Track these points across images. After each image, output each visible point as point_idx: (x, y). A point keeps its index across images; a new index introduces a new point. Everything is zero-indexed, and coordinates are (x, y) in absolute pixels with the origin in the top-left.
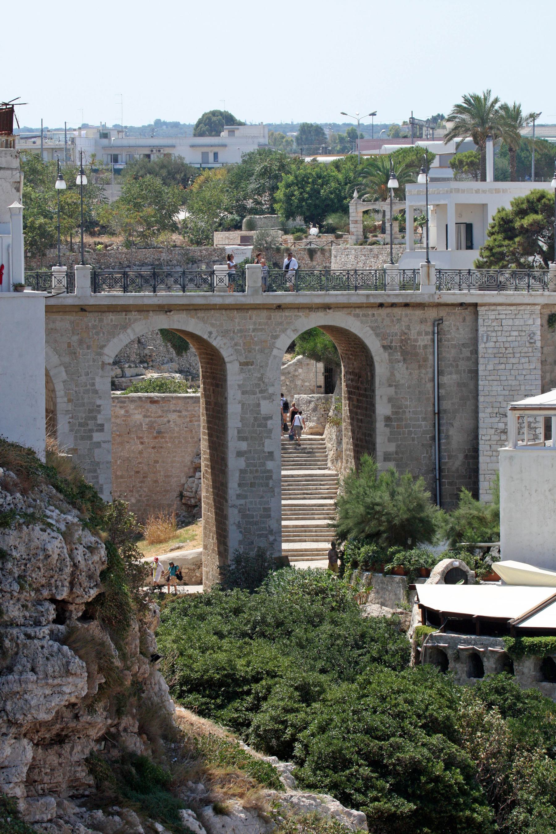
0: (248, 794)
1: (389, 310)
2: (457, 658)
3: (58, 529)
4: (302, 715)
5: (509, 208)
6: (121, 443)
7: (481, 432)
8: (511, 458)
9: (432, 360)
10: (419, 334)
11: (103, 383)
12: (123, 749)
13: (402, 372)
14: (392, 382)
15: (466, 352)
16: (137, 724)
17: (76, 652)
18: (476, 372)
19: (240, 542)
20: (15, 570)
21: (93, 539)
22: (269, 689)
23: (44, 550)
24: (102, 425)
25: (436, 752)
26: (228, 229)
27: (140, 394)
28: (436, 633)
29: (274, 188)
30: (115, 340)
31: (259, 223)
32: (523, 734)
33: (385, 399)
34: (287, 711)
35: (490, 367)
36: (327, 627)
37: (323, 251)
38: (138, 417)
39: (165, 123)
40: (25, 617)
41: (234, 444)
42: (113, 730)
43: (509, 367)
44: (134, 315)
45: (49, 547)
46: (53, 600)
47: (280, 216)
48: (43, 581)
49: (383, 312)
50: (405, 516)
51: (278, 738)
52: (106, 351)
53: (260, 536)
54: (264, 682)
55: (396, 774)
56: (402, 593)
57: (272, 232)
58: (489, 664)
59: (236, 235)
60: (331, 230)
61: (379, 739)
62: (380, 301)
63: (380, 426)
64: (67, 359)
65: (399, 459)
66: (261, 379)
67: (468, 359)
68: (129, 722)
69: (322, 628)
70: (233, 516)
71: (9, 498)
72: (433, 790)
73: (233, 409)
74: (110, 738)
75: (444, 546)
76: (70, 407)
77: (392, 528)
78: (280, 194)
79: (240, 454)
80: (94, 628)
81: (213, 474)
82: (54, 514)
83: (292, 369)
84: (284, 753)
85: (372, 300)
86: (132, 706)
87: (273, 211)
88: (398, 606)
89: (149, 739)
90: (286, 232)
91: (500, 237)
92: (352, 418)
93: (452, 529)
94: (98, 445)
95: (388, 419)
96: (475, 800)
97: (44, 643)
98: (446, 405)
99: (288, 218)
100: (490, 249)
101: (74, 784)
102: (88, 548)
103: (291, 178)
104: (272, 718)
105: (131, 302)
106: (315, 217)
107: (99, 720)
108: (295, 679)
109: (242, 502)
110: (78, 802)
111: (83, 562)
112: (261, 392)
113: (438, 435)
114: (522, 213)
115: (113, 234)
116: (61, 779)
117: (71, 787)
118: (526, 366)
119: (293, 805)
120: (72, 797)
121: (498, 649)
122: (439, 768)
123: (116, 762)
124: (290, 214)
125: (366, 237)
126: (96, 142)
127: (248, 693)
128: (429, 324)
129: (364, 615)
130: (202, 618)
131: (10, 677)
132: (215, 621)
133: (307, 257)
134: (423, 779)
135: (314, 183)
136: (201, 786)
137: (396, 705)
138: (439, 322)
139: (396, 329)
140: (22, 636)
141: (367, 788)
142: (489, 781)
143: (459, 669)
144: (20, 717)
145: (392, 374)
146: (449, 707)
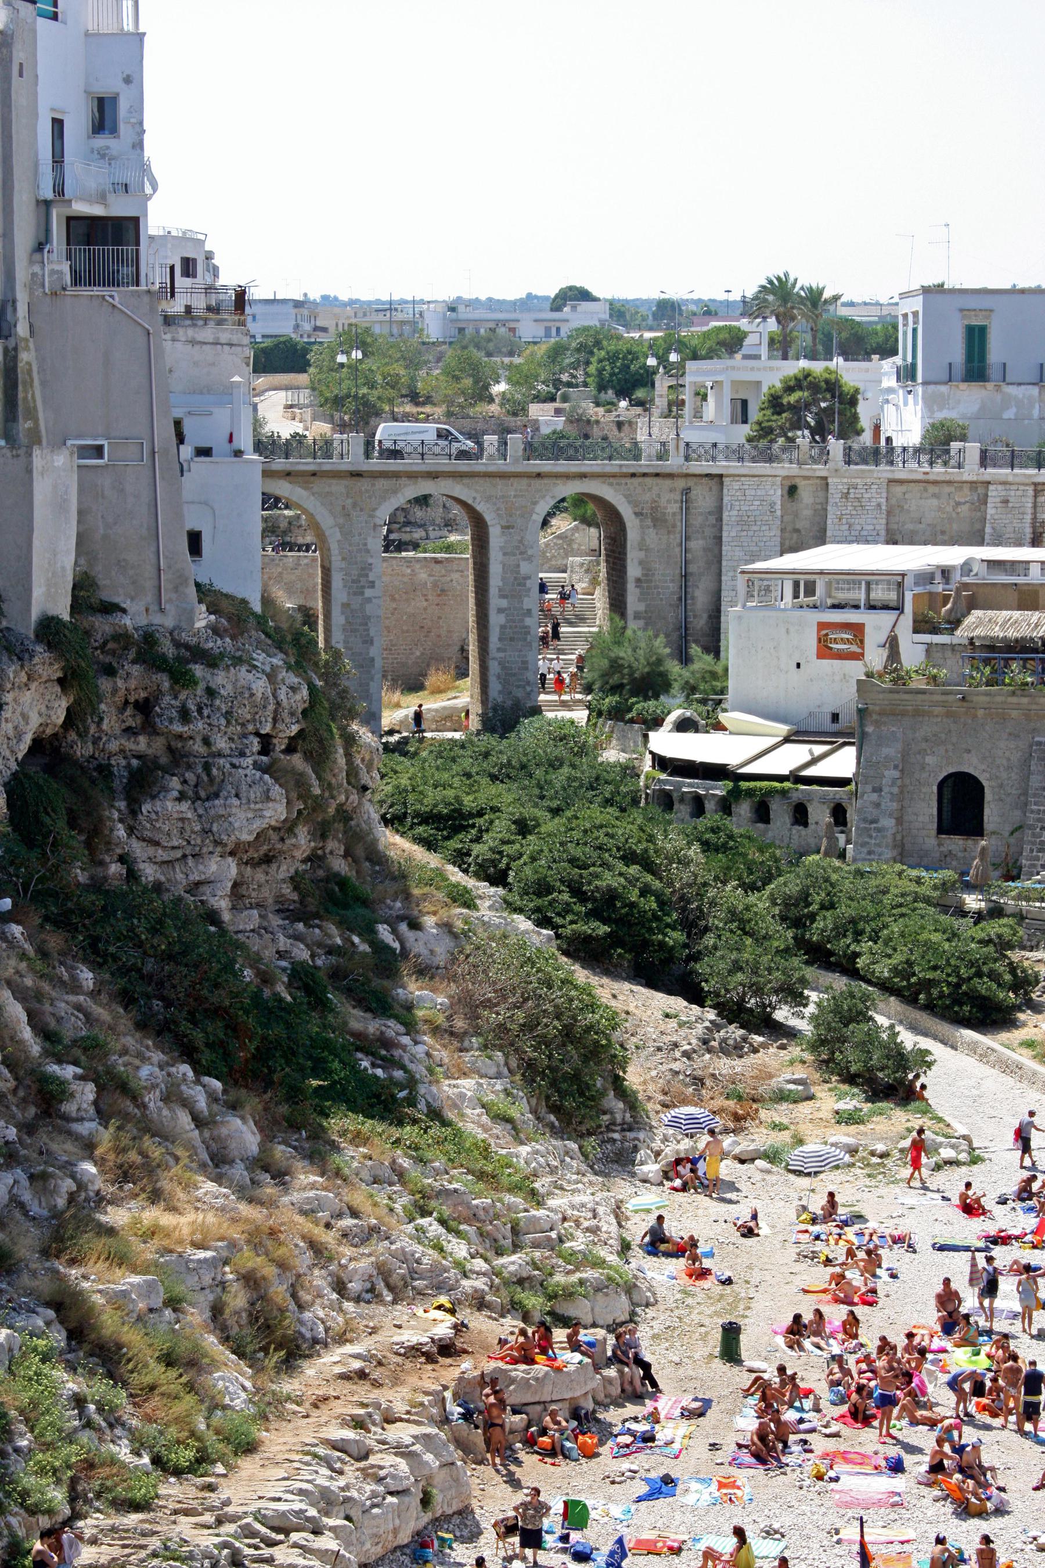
0: (441, 912)
1: (640, 479)
2: (682, 800)
3: (263, 671)
4: (517, 846)
5: (779, 385)
6: (407, 600)
7: (723, 594)
8: (740, 618)
9: (680, 526)
10: (669, 501)
11: (376, 543)
12: (329, 869)
13: (652, 537)
14: (642, 546)
15: (712, 519)
16: (343, 848)
17: (276, 780)
18: (721, 538)
19: (500, 692)
20: (223, 706)
21: (296, 680)
22: (491, 822)
23: (250, 689)
24: (373, 582)
25: (632, 881)
26: (544, 401)
27: (427, 555)
28: (663, 776)
29: (588, 363)
30: (387, 503)
31: (573, 396)
32: (729, 868)
33: (636, 562)
34: (504, 842)
35: (733, 534)
36: (566, 770)
37: (630, 423)
38: (423, 576)
39: (536, 297)
40: (231, 749)
41: (495, 601)
42: (320, 852)
43: (751, 533)
44: (404, 481)
45: (254, 686)
46: (257, 734)
47: (592, 389)
48: (249, 717)
49: (636, 481)
50: (646, 670)
51: (495, 867)
52: (378, 513)
53: (518, 687)
54: (486, 817)
55: (595, 900)
56: (640, 739)
57: (584, 405)
58: (710, 806)
59: (550, 407)
60: (641, 403)
61: (579, 868)
62: (632, 471)
63: (631, 586)
64: (341, 521)
65: (648, 619)
66: (521, 542)
67: (714, 526)
68: (334, 845)
69: (561, 771)
70: (494, 667)
71: (219, 642)
72: (627, 914)
73: (495, 570)
74: (315, 859)
75: (680, 699)
76: (343, 565)
77: (633, 681)
78: (592, 369)
79: (500, 611)
80: (297, 761)
81: (478, 629)
82: (261, 658)
83: (569, 534)
84: (498, 879)
85: (624, 470)
86: (337, 831)
87: (586, 385)
88: (634, 752)
89: (354, 861)
90: (598, 404)
91: (769, 412)
92: (608, 579)
93: (687, 683)
94: (369, 600)
95: (638, 580)
96: (668, 926)
97: (248, 772)
98: (693, 568)
99: (599, 391)
100: (759, 423)
101: (280, 899)
102: (291, 688)
103: (603, 353)
104: (490, 849)
105: (401, 468)
106: (624, 392)
107: (303, 842)
108: (513, 814)
109: (502, 655)
110: (283, 915)
111: (285, 701)
112: (521, 553)
113: (684, 597)
114: (789, 389)
115: (435, 405)
116: (267, 894)
117: (277, 902)
118: (767, 533)
119: (484, 923)
120: (278, 911)
121: (717, 792)
122: (634, 896)
123: (321, 881)
124: (602, 387)
125: (670, 411)
126: (445, 315)
127: (473, 826)
128: (678, 493)
129: (600, 759)
130: (454, 760)
131: (217, 802)
132: (466, 763)
133: (615, 429)
134: (619, 904)
135: (624, 358)
136: (398, 904)
137: (597, 838)
138: (687, 491)
139: (647, 497)
140: (228, 766)
141: (567, 912)
142: (684, 909)
143: (683, 810)
144: (225, 837)
145: (643, 539)
146: (648, 841)
